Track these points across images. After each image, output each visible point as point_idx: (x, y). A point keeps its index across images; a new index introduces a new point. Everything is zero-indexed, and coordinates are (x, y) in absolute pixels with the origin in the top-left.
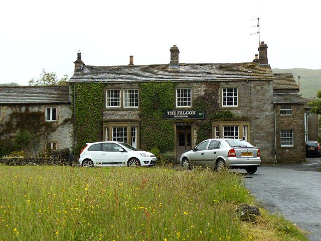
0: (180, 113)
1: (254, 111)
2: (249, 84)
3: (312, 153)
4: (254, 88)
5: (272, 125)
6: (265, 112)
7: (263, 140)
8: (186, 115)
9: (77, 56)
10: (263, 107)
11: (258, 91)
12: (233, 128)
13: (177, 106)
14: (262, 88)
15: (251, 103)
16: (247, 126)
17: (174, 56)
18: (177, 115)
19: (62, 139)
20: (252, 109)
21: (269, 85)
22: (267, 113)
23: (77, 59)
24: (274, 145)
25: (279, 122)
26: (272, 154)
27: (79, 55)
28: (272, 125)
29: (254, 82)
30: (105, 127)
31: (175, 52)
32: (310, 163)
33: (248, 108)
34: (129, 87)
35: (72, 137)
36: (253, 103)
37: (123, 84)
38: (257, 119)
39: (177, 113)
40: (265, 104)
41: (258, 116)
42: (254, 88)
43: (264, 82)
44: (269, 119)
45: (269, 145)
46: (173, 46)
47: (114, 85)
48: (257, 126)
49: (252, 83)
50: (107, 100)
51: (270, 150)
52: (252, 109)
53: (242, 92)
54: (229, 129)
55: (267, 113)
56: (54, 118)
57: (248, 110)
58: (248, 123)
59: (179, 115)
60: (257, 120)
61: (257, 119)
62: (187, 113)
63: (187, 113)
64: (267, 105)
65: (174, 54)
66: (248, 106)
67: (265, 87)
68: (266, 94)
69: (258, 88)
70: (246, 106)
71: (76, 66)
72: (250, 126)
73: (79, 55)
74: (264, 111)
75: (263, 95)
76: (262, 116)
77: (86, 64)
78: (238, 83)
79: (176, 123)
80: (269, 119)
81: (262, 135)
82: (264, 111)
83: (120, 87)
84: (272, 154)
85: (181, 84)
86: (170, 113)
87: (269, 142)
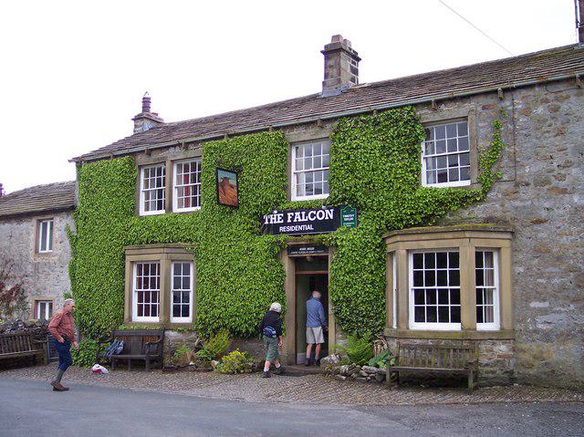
2: (507, 103)
4: (526, 112)
8: (309, 222)
9: (141, 105)
10: (562, 178)
11: (541, 121)
12: (442, 257)
13: (295, 198)
14: (556, 109)
16: (499, 249)
17: (331, 67)
18: (285, 224)
20: (522, 189)
22: (576, 199)
23: (140, 111)
29: (524, 92)
31: (337, 52)
34: (182, 156)
38: (539, 222)
39: (285, 218)
40: (568, 165)
41: (544, 214)
42: (526, 112)
43: (561, 87)
46: (329, 41)
48: (540, 251)
49: (518, 96)
54: (430, 264)
55: (576, 199)
56: (50, 249)
57: (506, 194)
59: (292, 224)
60: (537, 227)
61: (539, 222)
62: (313, 216)
63: (313, 216)
65: (331, 62)
66: (505, 178)
67: (564, 106)
69: (540, 110)
71: (136, 126)
72: (514, 250)
73: (146, 102)
74: (564, 191)
81: (556, 281)
82: (564, 191)
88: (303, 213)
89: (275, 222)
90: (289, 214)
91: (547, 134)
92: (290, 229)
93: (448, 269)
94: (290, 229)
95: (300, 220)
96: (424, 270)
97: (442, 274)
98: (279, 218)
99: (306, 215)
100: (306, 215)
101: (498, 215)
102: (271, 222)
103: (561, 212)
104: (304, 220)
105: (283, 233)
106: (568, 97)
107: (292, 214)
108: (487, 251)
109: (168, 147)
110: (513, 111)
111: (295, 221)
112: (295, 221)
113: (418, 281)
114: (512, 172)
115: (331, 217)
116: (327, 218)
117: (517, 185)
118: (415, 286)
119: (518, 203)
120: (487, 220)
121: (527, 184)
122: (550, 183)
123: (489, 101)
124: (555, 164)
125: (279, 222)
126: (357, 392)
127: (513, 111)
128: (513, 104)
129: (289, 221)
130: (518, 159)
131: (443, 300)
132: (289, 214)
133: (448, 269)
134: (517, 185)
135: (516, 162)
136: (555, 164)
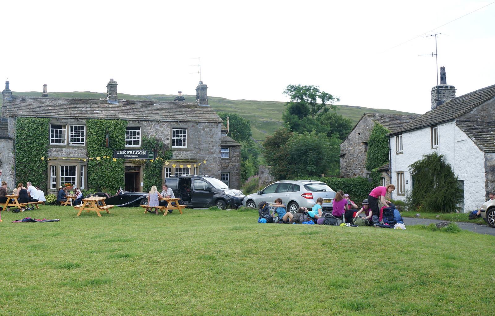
4: (203, 129)
14: (211, 130)
18: (126, 155)
20: (201, 151)
22: (215, 155)
39: (126, 153)
42: (203, 129)
49: (202, 124)
59: (129, 155)
62: (138, 153)
63: (138, 153)
66: (197, 147)
67: (213, 130)
82: (212, 153)
88: (134, 152)
89: (122, 154)
90: (128, 151)
91: (209, 137)
92: (128, 156)
93: (72, 171)
94: (128, 156)
95: (132, 154)
96: (64, 171)
97: (70, 173)
98: (124, 152)
99: (135, 152)
100: (135, 152)
101: (194, 158)
102: (120, 154)
103: (211, 158)
104: (134, 154)
105: (125, 157)
106: (214, 127)
108: (65, 164)
109: (206, 122)
110: (200, 128)
111: (130, 154)
112: (130, 154)
113: (62, 174)
114: (199, 146)
115: (145, 154)
117: (200, 150)
118: (61, 176)
119: (200, 155)
120: (192, 159)
121: (203, 150)
122: (209, 150)
123: (195, 124)
124: (210, 145)
125: (124, 154)
126: (249, 213)
127: (200, 128)
128: (200, 127)
129: (128, 154)
130: (201, 143)
131: (70, 180)
132: (128, 151)
133: (72, 171)
134: (200, 150)
135: (200, 143)
136: (210, 145)
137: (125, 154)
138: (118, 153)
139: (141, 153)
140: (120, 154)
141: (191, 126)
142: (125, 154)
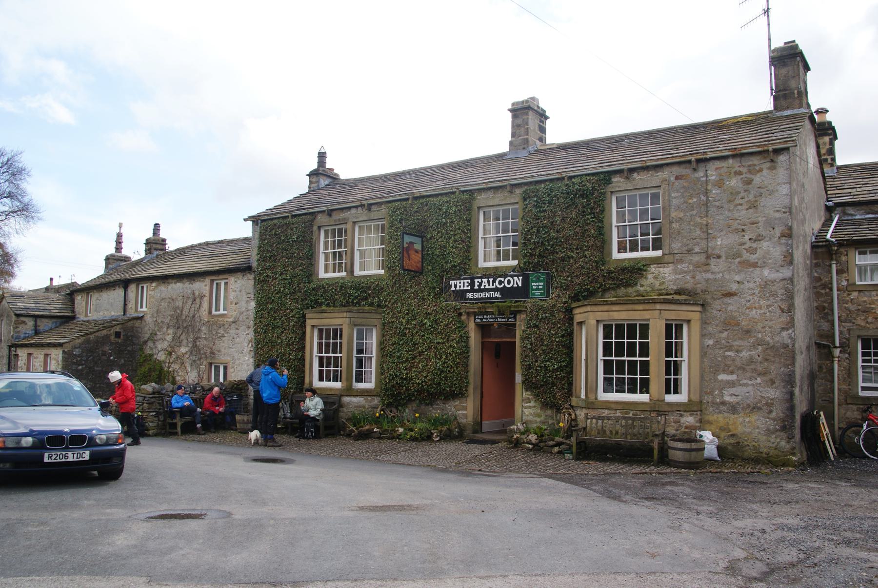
0: (480, 284)
1: (719, 267)
2: (701, 174)
3: (2, 212)
4: (719, 184)
5: (785, 318)
6: (757, 271)
7: (748, 375)
9: (316, 160)
11: (734, 193)
12: (632, 328)
14: (749, 182)
15: (708, 237)
16: (689, 321)
18: (472, 290)
19: (236, 356)
21: (772, 168)
22: (766, 272)
24: (792, 394)
25: (852, 307)
26: (783, 428)
27: (322, 156)
28: (785, 318)
29: (718, 164)
30: (313, 326)
32: (465, 353)
33: (696, 258)
35: (252, 354)
36: (715, 238)
37: (353, 211)
38: (730, 295)
39: (472, 284)
40: (759, 239)
41: (734, 287)
42: (719, 184)
43: (755, 160)
44: (774, 295)
45: (774, 393)
47: (334, 213)
48: (730, 323)
49: (712, 167)
50: (860, 371)
51: (778, 412)
52: (713, 261)
53: (674, 202)
57: (697, 266)
58: (693, 313)
59: (480, 290)
60: (727, 300)
61: (730, 295)
64: (765, 244)
66: (697, 250)
67: (757, 179)
68: (763, 201)
69: (734, 182)
70: (690, 252)
71: (311, 182)
72: (704, 323)
75: (753, 206)
76: (747, 285)
77: (343, 176)
78: (665, 174)
79: (475, 314)
80: (774, 295)
81: (745, 354)
82: (755, 265)
83: (345, 219)
84: (783, 428)
85: (490, 194)
86: (456, 286)
87: (773, 382)
90: (476, 281)
98: (466, 284)
99: (494, 282)
104: (491, 287)
107: (480, 280)
111: (482, 287)
116: (515, 285)
125: (466, 288)
132: (476, 281)
137: (469, 288)
138: (453, 288)
139: (509, 282)
140: (458, 288)
141: (672, 179)
142: (469, 288)
